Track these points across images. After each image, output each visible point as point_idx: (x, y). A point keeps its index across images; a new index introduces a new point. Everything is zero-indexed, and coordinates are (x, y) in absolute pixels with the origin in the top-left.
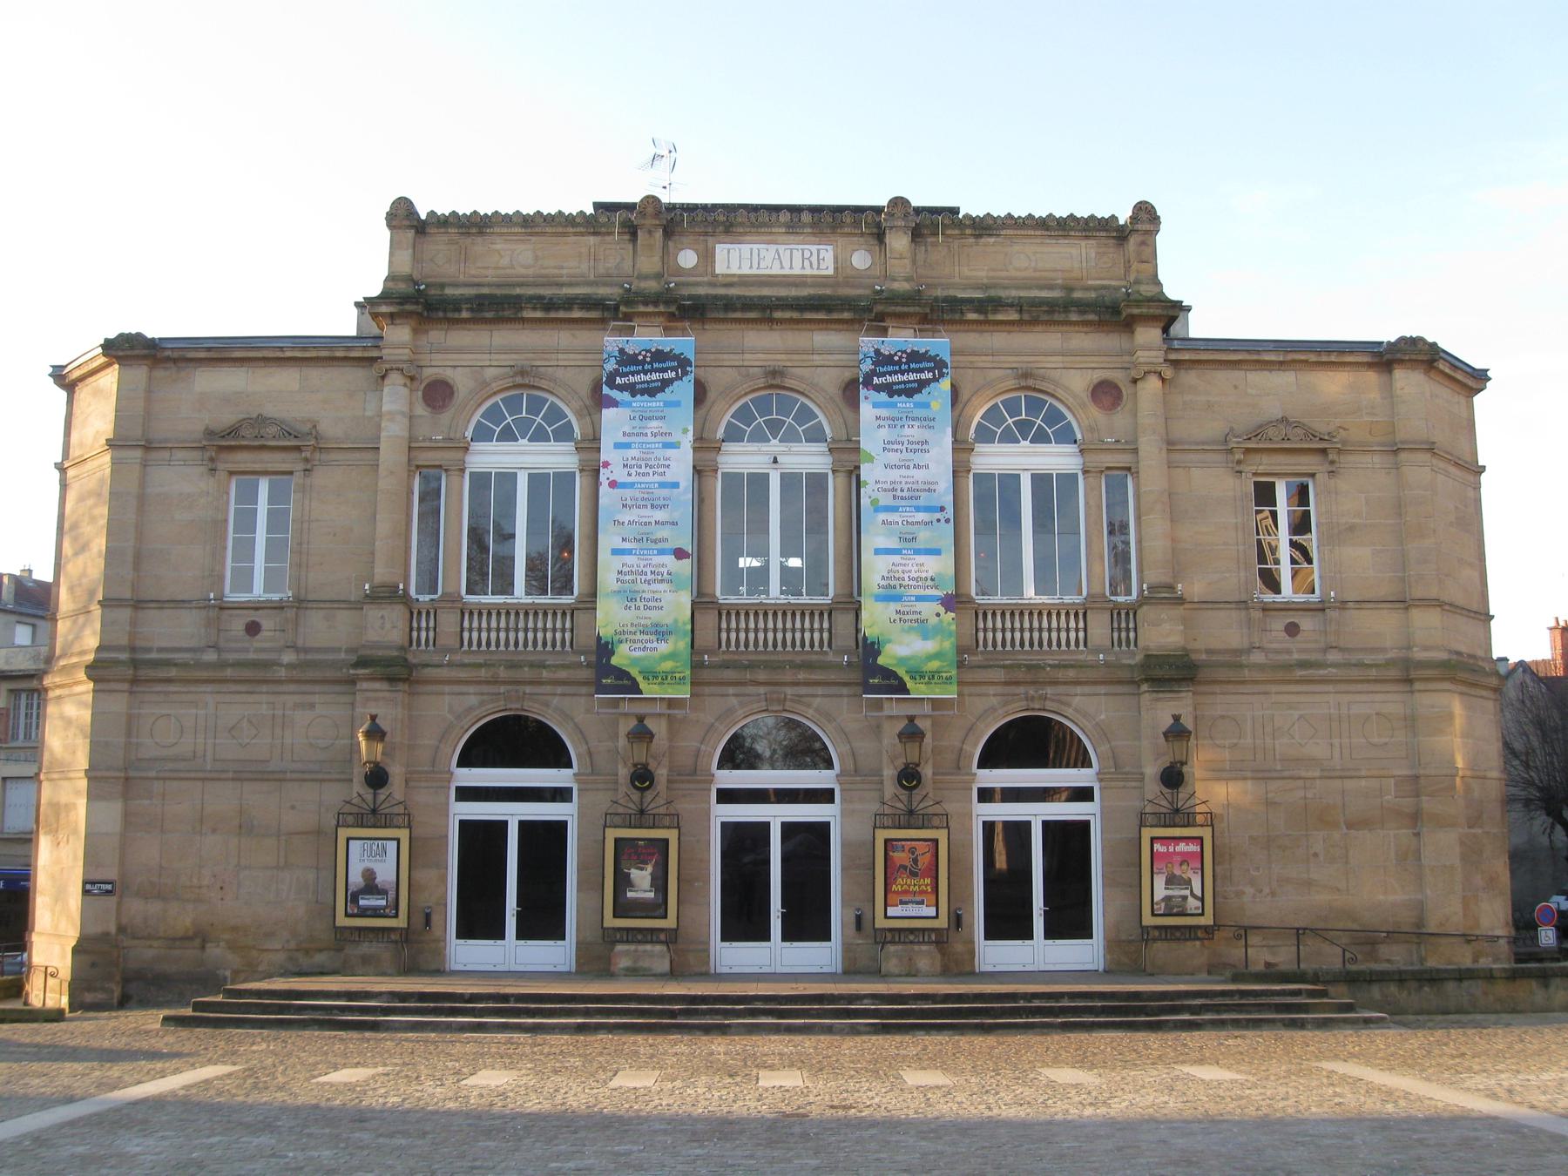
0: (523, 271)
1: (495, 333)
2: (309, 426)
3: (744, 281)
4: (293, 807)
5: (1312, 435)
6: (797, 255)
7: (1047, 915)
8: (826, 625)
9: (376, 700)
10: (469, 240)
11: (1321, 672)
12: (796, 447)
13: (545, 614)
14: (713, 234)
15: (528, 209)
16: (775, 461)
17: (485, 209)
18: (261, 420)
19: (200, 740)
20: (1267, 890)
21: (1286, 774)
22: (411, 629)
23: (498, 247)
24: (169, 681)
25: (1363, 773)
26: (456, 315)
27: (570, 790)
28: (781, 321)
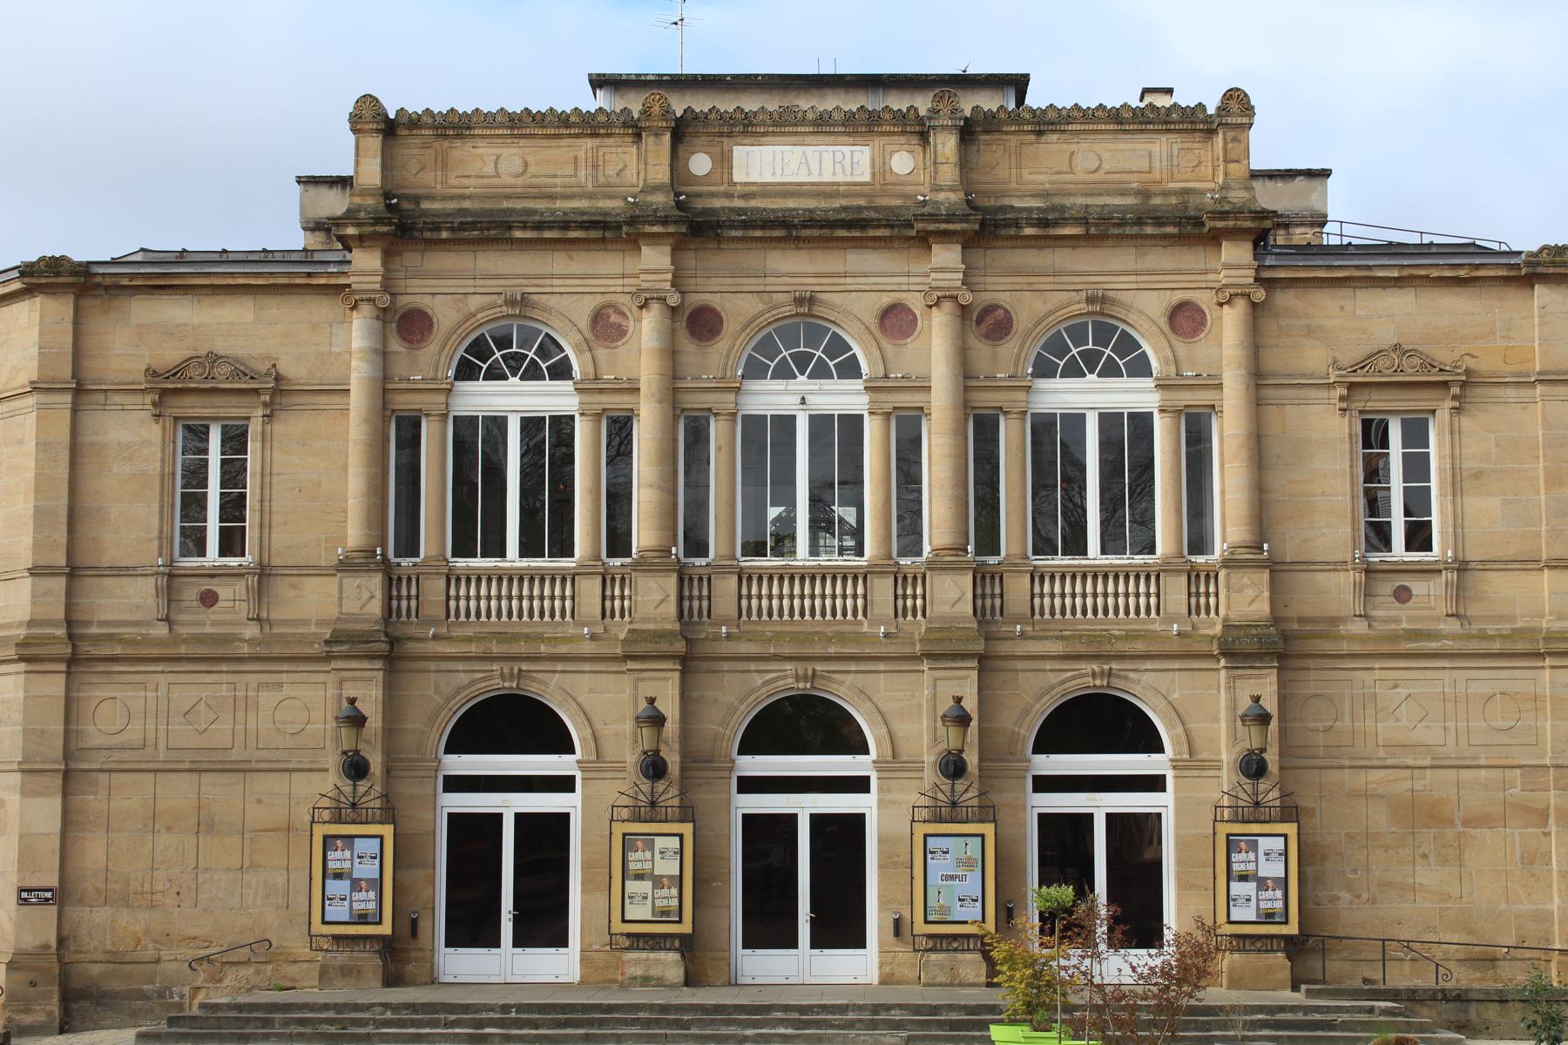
0: (512, 181)
1: (480, 255)
2: (268, 365)
3: (766, 190)
4: (259, 801)
5: (240, 373)
6: (827, 157)
7: (814, 923)
8: (860, 590)
9: (354, 679)
10: (446, 144)
11: (1434, 645)
12: (826, 384)
13: (511, 580)
14: (730, 135)
15: (515, 107)
16: (803, 401)
17: (466, 107)
18: (214, 358)
19: (151, 727)
20: (1365, 896)
21: (1390, 762)
22: (390, 598)
23: (480, 151)
24: (113, 659)
25: (1483, 762)
26: (435, 235)
27: (867, 778)
28: (808, 240)
